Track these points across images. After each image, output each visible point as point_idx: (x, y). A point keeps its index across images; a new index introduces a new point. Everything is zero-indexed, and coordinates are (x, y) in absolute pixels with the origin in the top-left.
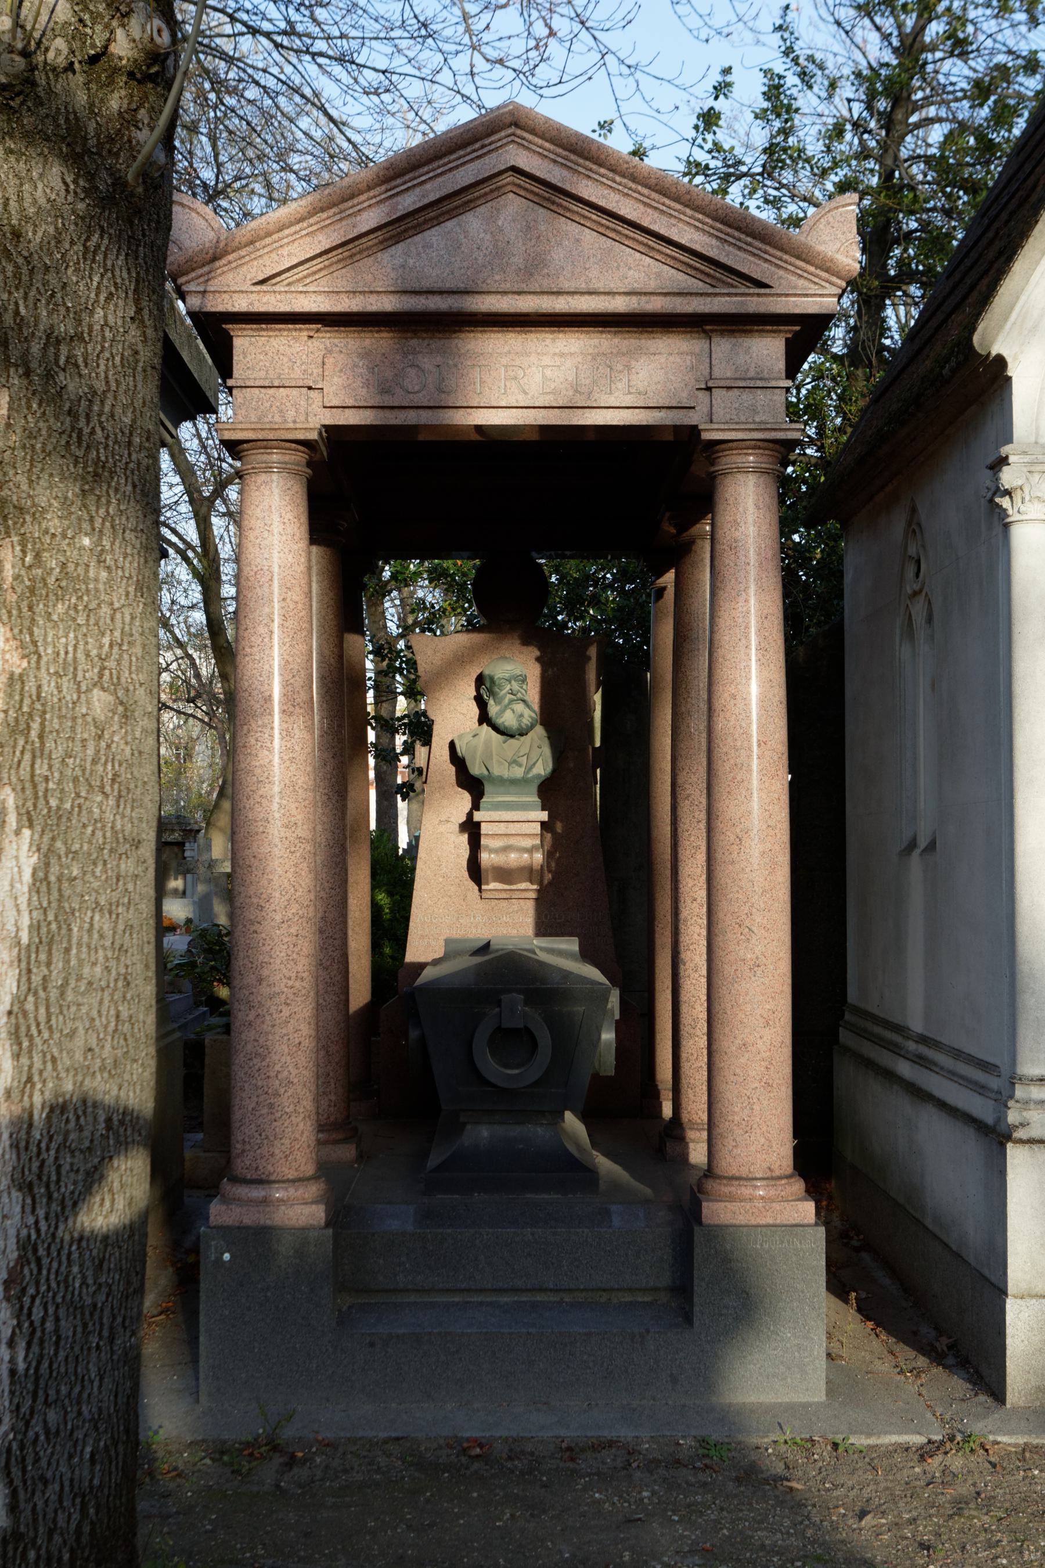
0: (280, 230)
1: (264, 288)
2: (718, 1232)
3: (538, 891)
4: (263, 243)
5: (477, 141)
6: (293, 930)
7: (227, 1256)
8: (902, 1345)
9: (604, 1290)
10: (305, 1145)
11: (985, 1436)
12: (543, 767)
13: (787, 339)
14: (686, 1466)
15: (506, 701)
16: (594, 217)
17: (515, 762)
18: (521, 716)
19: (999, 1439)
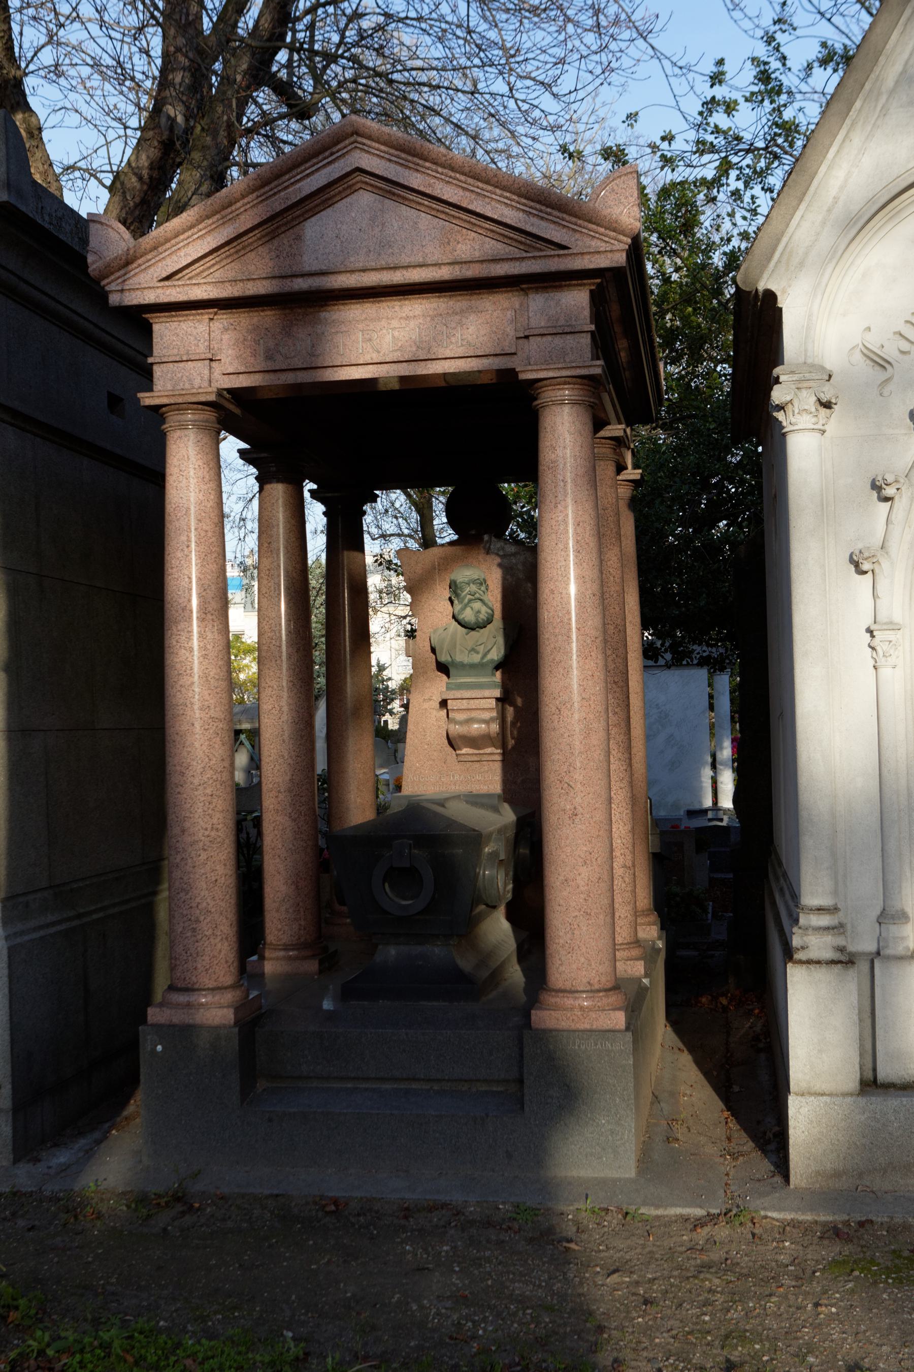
0: (176, 236)
1: (166, 283)
2: (545, 1036)
3: (503, 754)
4: (164, 248)
5: (326, 150)
6: (209, 791)
7: (159, 1048)
8: (743, 1133)
9: (466, 1081)
10: (223, 961)
11: (756, 1211)
12: (496, 653)
13: (591, 291)
14: (494, 1227)
15: (466, 600)
16: (426, 203)
17: (473, 650)
18: (479, 612)
19: (770, 1214)
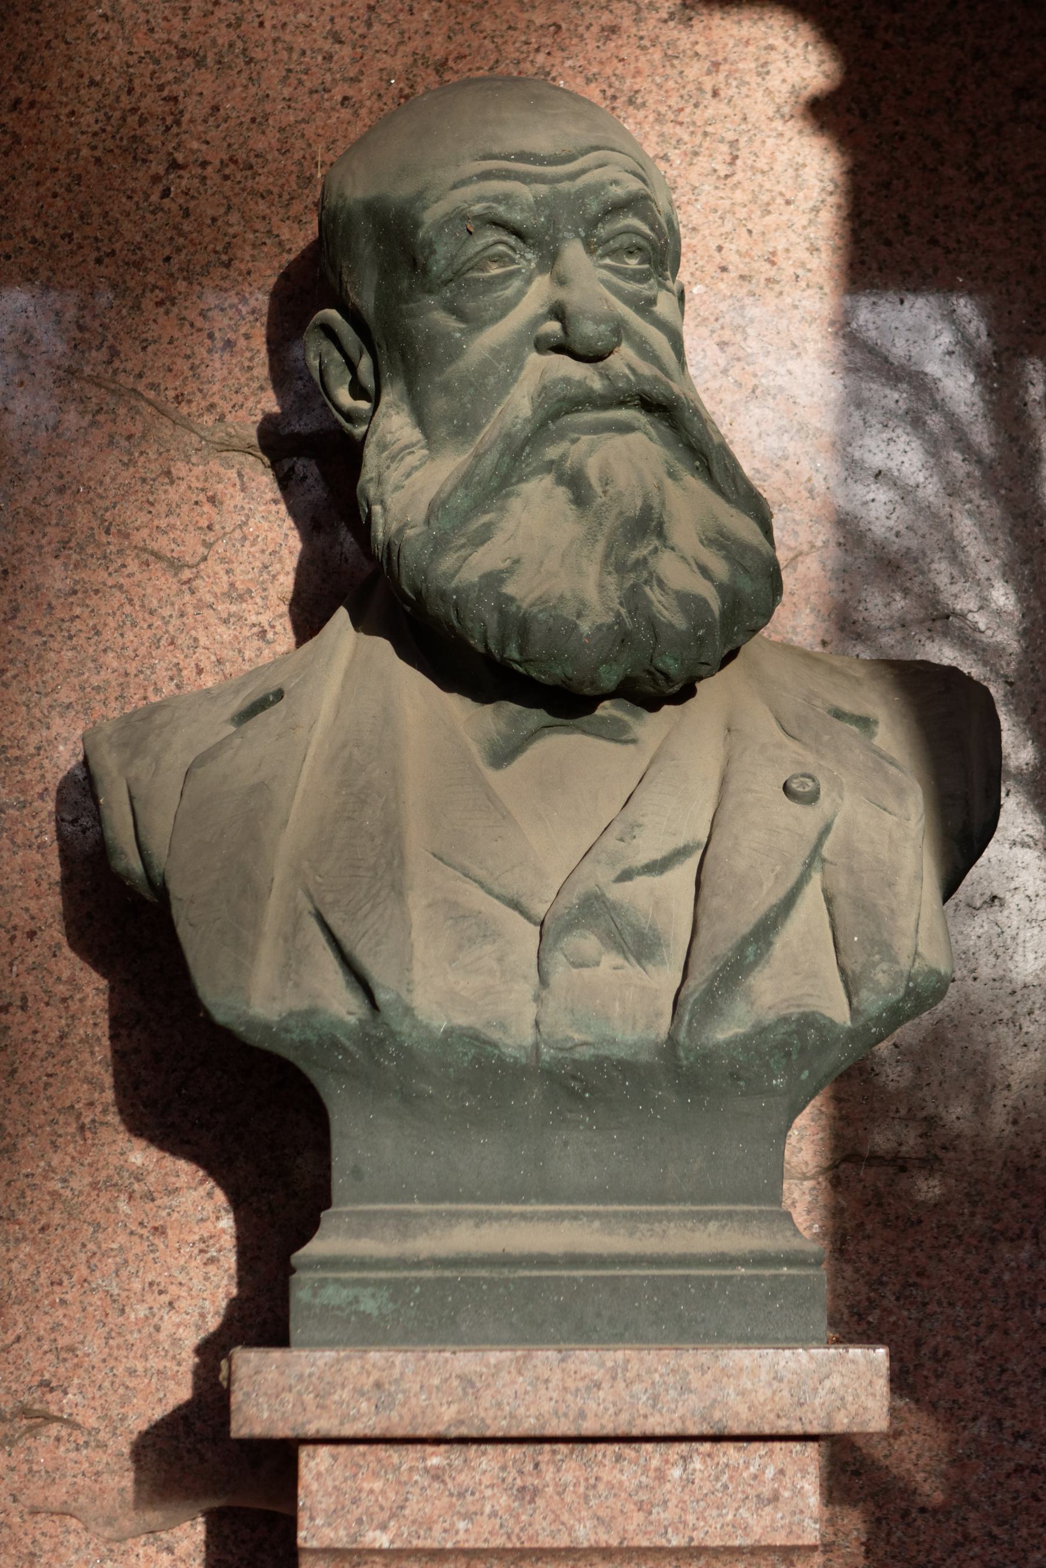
1: (377, 336)
15: (520, 403)
18: (647, 524)
